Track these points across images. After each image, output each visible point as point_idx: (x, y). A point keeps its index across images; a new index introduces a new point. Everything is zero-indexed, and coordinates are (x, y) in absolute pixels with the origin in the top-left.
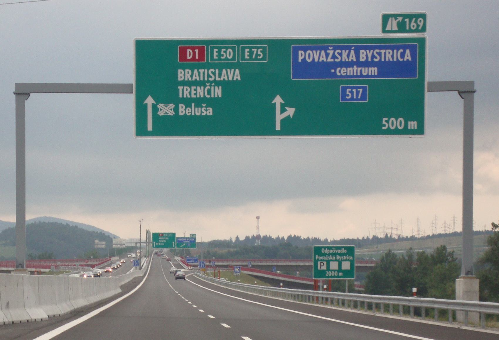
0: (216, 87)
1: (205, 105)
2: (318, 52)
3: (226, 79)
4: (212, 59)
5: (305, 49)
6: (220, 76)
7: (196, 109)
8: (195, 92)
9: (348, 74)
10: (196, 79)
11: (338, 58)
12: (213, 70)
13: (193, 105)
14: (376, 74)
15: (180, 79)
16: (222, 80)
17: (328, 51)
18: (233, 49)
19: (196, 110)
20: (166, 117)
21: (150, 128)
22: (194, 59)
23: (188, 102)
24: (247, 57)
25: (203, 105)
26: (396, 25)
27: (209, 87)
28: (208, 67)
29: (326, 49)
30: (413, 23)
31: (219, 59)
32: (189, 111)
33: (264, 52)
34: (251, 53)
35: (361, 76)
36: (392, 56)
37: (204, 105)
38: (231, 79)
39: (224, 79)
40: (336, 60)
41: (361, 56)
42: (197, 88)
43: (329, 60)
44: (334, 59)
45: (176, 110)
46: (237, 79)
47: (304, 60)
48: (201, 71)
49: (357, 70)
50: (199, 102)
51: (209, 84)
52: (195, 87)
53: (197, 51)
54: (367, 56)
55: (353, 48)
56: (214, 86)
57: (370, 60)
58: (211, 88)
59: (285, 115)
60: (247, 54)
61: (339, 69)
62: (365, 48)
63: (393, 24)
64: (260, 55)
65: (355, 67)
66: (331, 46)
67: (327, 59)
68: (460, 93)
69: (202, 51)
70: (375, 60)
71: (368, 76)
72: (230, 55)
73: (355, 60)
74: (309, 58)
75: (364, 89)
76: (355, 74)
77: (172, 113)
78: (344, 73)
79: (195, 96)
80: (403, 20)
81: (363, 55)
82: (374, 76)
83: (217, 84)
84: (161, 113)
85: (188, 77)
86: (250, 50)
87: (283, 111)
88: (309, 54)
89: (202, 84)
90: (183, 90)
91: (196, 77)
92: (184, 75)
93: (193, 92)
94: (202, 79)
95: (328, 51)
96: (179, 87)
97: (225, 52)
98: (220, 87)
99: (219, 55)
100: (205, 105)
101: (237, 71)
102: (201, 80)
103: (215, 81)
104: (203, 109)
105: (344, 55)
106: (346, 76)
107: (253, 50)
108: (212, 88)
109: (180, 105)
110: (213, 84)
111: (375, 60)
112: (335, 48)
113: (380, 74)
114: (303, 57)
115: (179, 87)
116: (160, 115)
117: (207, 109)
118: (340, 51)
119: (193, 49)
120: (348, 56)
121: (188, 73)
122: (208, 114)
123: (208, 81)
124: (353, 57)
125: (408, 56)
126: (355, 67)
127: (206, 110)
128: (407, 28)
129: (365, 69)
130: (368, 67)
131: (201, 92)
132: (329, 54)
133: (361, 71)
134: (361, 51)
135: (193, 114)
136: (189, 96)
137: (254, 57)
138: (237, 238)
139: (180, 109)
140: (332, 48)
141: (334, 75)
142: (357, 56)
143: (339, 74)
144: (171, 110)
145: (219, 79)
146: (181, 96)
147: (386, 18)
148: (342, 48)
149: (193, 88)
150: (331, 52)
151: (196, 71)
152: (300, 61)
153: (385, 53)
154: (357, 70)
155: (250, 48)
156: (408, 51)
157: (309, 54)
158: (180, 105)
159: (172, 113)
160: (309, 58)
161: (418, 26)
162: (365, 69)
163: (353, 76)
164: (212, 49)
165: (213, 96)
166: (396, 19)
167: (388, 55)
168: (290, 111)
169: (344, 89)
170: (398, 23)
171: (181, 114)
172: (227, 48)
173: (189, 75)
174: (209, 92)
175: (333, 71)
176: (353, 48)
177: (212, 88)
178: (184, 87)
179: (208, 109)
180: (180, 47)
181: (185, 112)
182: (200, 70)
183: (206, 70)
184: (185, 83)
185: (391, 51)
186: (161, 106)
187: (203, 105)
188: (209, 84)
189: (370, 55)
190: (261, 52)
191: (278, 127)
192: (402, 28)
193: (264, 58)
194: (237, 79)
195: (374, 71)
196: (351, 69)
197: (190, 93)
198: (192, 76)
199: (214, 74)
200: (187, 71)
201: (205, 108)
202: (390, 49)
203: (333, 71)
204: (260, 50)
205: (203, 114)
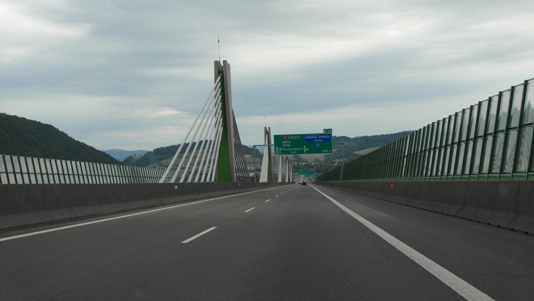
19: (96, 178)
21: (277, 153)
23: (285, 148)
29: (311, 136)
35: (320, 141)
43: (312, 138)
59: (306, 150)
75: (320, 144)
87: (306, 149)
99: (290, 138)
102: (30, 158)
105: (315, 137)
113: (323, 141)
125: (329, 137)
138: (357, 137)
141: (314, 141)
147: (324, 130)
159: (295, 148)
168: (307, 149)
169: (316, 144)
191: (305, 152)
192: (327, 131)
195: (322, 140)
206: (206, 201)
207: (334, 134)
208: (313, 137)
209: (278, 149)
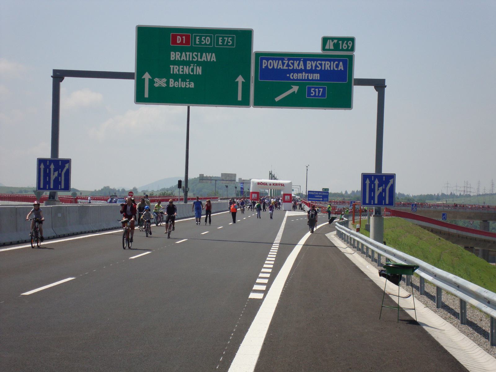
0: (198, 67)
1: (189, 80)
2: (277, 61)
3: (206, 60)
4: (195, 44)
5: (267, 60)
6: (201, 58)
7: (182, 83)
8: (182, 70)
9: (299, 78)
10: (183, 60)
11: (291, 67)
12: (196, 54)
13: (180, 80)
14: (319, 79)
15: (172, 59)
16: (202, 60)
17: (284, 61)
18: (211, 37)
20: (160, 88)
21: (146, 95)
22: (182, 43)
23: (176, 77)
24: (220, 43)
25: (187, 80)
26: (332, 44)
27: (193, 67)
28: (193, 50)
29: (283, 60)
30: (344, 45)
31: (200, 44)
32: (177, 84)
34: (223, 40)
35: (308, 80)
36: (330, 67)
37: (188, 80)
38: (209, 60)
39: (204, 60)
40: (290, 68)
41: (308, 65)
42: (183, 67)
43: (285, 68)
44: (288, 67)
45: (168, 83)
46: (213, 61)
47: (267, 67)
48: (188, 53)
49: (305, 75)
50: (184, 78)
51: (193, 65)
52: (182, 67)
53: (184, 37)
54: (312, 66)
55: (302, 59)
56: (196, 66)
57: (314, 68)
58: (194, 68)
60: (220, 41)
61: (292, 74)
62: (311, 60)
63: (330, 45)
64: (230, 42)
65: (304, 73)
66: (286, 58)
67: (283, 67)
69: (188, 37)
70: (317, 69)
71: (312, 80)
72: (208, 41)
73: (303, 68)
74: (270, 66)
76: (304, 78)
77: (164, 85)
78: (296, 77)
79: (182, 73)
80: (338, 42)
81: (320, 193)
82: (317, 80)
83: (198, 64)
84: (156, 85)
85: (178, 57)
86: (222, 38)
88: (270, 63)
90: (173, 68)
91: (183, 58)
92: (175, 56)
93: (181, 70)
94: (188, 60)
95: (284, 61)
96: (171, 66)
97: (205, 39)
98: (201, 67)
99: (200, 41)
100: (189, 80)
101: (214, 54)
104: (187, 83)
106: (297, 80)
107: (225, 38)
108: (195, 67)
109: (171, 80)
110: (196, 65)
111: (317, 69)
112: (289, 60)
114: (266, 65)
115: (171, 66)
116: (156, 86)
117: (190, 83)
118: (292, 62)
119: (181, 36)
120: (298, 65)
121: (178, 54)
122: (191, 87)
124: (302, 66)
125: (327, 194)
126: (304, 73)
127: (189, 84)
128: (341, 48)
129: (311, 75)
130: (313, 73)
131: (187, 70)
132: (285, 63)
133: (308, 76)
134: (308, 62)
135: (180, 86)
136: (178, 73)
137: (225, 44)
138: (346, 192)
139: (171, 83)
140: (287, 59)
141: (289, 79)
142: (305, 65)
143: (292, 78)
144: (164, 83)
145: (200, 60)
146: (172, 73)
147: (323, 189)
148: (294, 60)
149: (181, 67)
150: (286, 62)
151: (184, 53)
152: (264, 67)
153: (325, 64)
154: (305, 75)
155: (223, 37)
156: (341, 63)
157: (270, 63)
158: (171, 80)
160: (270, 66)
161: (348, 47)
162: (311, 75)
163: (302, 80)
164: (195, 36)
165: (195, 73)
166: (332, 41)
167: (327, 66)
170: (334, 44)
171: (171, 86)
172: (206, 36)
173: (179, 57)
174: (193, 71)
175: (288, 75)
176: (302, 59)
177: (195, 67)
178: (175, 66)
179: (191, 83)
180: (172, 34)
181: (174, 85)
182: (187, 53)
183: (191, 53)
184: (176, 63)
185: (329, 63)
186: (156, 80)
187: (187, 80)
188: (193, 65)
189: (314, 65)
190: (230, 40)
192: (336, 47)
193: (233, 45)
194: (213, 61)
195: (317, 76)
196: (301, 74)
197: (179, 71)
198: (181, 57)
199: (197, 56)
200: (177, 53)
201: (188, 83)
202: (329, 61)
203: (288, 75)
204: (230, 38)
205: (187, 87)
206: (179, 221)
207: (330, 192)
208: (288, 65)
209: (151, 82)
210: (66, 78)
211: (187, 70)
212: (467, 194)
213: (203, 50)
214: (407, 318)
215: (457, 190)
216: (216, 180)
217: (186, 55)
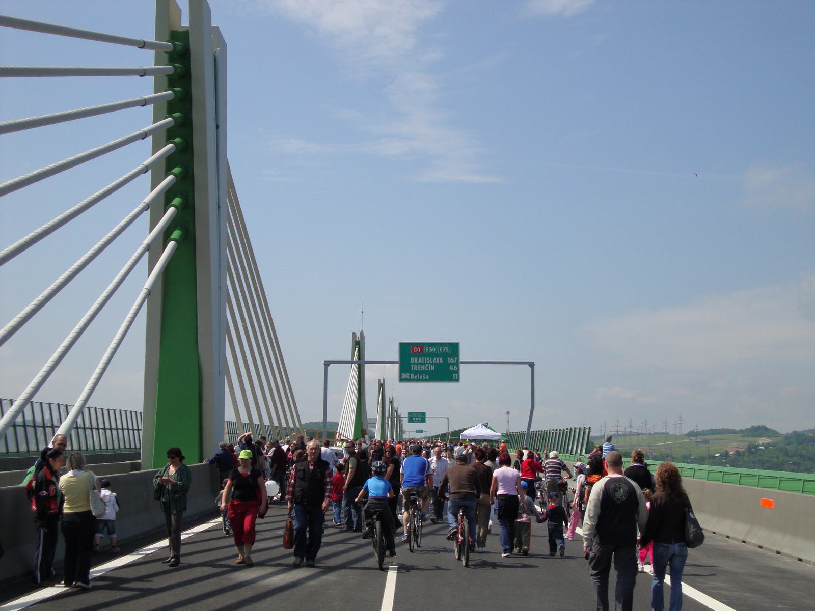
28: (426, 356)
33: (449, 349)
48: (423, 358)
53: (419, 348)
68: (529, 365)
69: (421, 348)
83: (432, 364)
85: (416, 361)
89: (424, 364)
91: (420, 361)
93: (419, 368)
99: (429, 350)
101: (441, 358)
103: (430, 363)
115: (442, 362)
123: (427, 363)
172: (432, 347)
174: (428, 368)
184: (414, 364)
193: (449, 352)
197: (417, 368)
199: (430, 359)
210: (331, 364)
211: (423, 368)
212: (634, 457)
213: (432, 356)
214: (161, 239)
215: (601, 430)
216: (409, 432)
217: (422, 359)
